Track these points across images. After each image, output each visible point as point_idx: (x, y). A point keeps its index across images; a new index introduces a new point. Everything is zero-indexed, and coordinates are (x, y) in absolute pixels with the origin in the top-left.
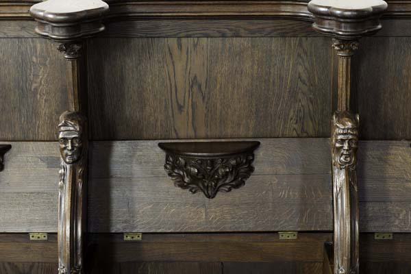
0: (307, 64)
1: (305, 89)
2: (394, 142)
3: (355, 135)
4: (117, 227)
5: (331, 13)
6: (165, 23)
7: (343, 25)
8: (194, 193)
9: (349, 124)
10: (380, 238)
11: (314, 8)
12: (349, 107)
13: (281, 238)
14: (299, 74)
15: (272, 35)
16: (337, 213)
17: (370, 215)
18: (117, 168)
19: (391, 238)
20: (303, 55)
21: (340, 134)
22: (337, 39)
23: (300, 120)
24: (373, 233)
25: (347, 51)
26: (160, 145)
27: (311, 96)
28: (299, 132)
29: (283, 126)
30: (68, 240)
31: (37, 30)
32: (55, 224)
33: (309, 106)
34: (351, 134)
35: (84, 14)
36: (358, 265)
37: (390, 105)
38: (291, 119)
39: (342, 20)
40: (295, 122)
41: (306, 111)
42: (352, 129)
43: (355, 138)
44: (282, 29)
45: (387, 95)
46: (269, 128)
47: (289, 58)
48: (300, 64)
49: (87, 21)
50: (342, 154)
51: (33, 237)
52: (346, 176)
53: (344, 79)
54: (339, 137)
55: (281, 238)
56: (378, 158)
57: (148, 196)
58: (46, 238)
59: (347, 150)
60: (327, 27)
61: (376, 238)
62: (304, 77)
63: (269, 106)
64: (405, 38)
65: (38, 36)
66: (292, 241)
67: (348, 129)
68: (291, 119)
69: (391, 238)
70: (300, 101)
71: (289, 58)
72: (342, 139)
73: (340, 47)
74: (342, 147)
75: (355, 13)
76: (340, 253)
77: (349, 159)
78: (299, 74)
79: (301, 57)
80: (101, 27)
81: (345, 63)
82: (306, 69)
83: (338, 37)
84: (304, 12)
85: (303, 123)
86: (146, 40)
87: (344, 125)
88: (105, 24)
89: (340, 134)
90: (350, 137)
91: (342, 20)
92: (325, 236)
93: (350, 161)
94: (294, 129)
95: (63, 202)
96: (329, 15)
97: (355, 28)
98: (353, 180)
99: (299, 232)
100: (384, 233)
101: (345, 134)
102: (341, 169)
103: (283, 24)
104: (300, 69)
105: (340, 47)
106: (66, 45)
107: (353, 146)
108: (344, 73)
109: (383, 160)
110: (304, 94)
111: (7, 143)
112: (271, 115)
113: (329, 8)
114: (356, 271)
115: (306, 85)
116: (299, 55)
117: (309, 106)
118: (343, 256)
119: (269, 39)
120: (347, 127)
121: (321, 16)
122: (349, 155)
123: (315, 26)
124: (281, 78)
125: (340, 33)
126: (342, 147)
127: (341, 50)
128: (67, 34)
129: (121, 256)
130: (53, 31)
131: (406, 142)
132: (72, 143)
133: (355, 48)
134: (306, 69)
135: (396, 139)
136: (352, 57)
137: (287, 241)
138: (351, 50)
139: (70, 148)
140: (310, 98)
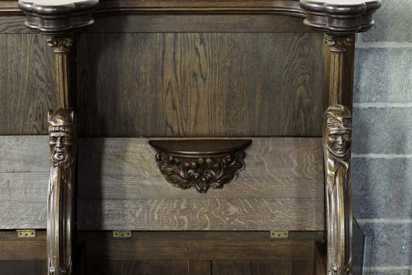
0: (43, 61)
1: (43, 85)
2: (133, 139)
3: (67, 132)
4: (108, 224)
5: (33, 9)
6: (160, 20)
7: (46, 21)
8: (206, 191)
9: (61, 122)
10: (119, 235)
11: (304, 4)
12: (67, 104)
13: (19, 236)
14: (37, 71)
15: (7, 31)
16: (330, 214)
17: (106, 213)
18: (246, 162)
19: (130, 235)
20: (39, 52)
21: (52, 132)
22: (329, 34)
23: (40, 116)
24: (111, 231)
25: (62, 47)
26: (151, 143)
27: (50, 93)
28: (39, 130)
29: (23, 123)
30: (57, 235)
31: (27, 23)
32: (44, 221)
33: (48, 103)
34: (63, 132)
35: (67, 9)
36: (70, 263)
37: (129, 102)
38: (31, 116)
39: (334, 16)
40: (34, 119)
41: (46, 107)
42: (64, 127)
43: (68, 135)
44: (16, 26)
45: (125, 92)
46: (9, 125)
47: (26, 56)
48: (37, 61)
49: (76, 14)
50: (56, 152)
51: (273, 234)
52: (58, 174)
53: (61, 76)
54: (52, 135)
55: (19, 236)
56: (115, 155)
57: (144, 195)
58: (287, 236)
59: (341, 145)
60: (319, 22)
61: (114, 236)
62: (41, 73)
63: (8, 102)
64: (142, 34)
65: (28, 30)
66: (31, 239)
67: (59, 127)
68: (31, 116)
69: (130, 235)
70: (39, 98)
71: (26, 56)
72: (54, 137)
73: (53, 44)
74: (55, 144)
75: (348, 9)
76: (51, 251)
77: (62, 157)
78: (37, 71)
79: (37, 54)
80: (90, 20)
81: (60, 60)
82: (43, 66)
83: (330, 33)
84: (296, 8)
85: (43, 121)
86: (215, 34)
87: (56, 122)
88: (95, 17)
89: (52, 132)
90: (62, 134)
91: (334, 16)
92: (268, 233)
93: (63, 159)
94: (34, 126)
95: (52, 198)
96: (323, 11)
97: (57, 25)
98: (67, 178)
99: (37, 230)
100: (122, 231)
101: (57, 131)
102: (55, 167)
103: (17, 21)
104: (37, 65)
105: (53, 44)
106: (57, 37)
107: (66, 143)
108: (60, 70)
109: (121, 156)
110: (42, 90)
111: (249, 138)
112: (10, 113)
113: (322, 4)
114: (68, 270)
115: (44, 82)
116: (35, 52)
117: (48, 103)
118: (54, 253)
119: (4, 35)
120: (58, 125)
121: (311, 12)
122: (62, 153)
123: (306, 22)
124: (19, 75)
125: (43, 30)
126: (55, 144)
127: (55, 46)
128: (56, 27)
129: (117, 252)
130: (43, 24)
131: (145, 139)
132: (61, 141)
133: (68, 45)
134: (43, 66)
135: (134, 137)
136: (67, 53)
137: (24, 239)
138: (65, 46)
139: (58, 145)
140: (49, 95)
